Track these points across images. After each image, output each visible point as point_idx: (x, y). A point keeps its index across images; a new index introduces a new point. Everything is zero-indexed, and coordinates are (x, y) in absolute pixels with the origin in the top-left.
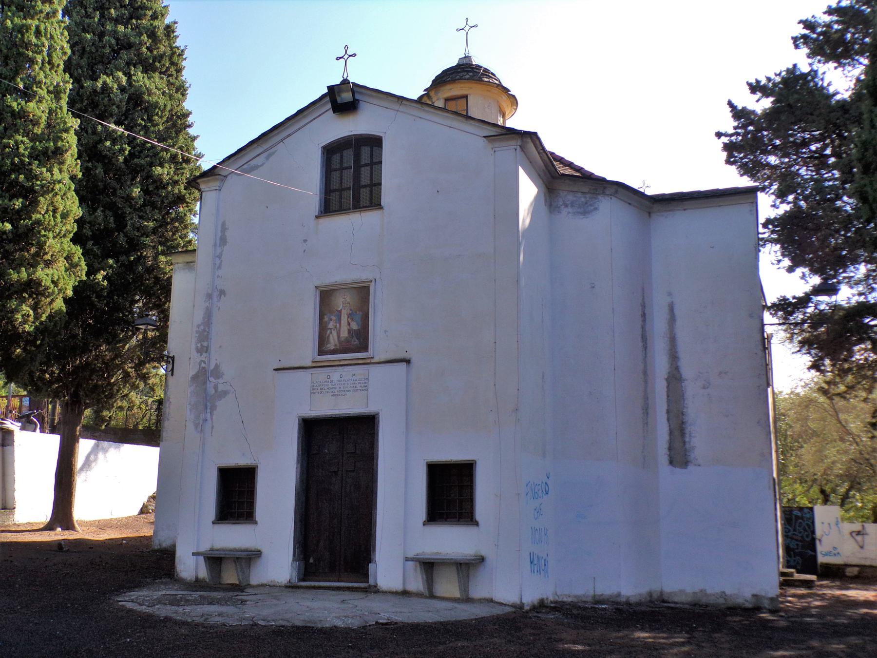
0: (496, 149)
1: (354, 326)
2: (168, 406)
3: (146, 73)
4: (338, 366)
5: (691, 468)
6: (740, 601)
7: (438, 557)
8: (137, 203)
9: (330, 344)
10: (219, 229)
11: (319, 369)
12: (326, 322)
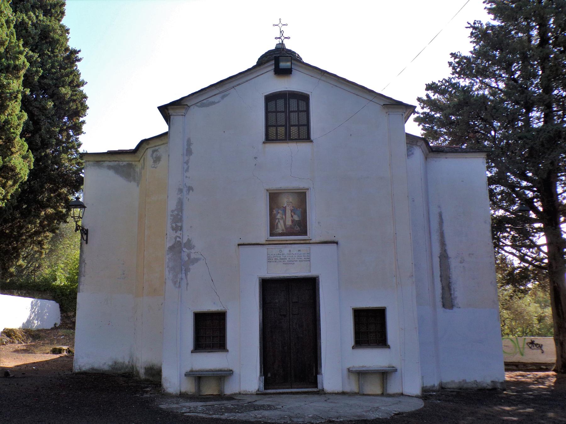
0: (390, 113)
1: (296, 218)
2: (83, 266)
3: (46, 16)
4: (287, 244)
5: (455, 309)
6: (485, 385)
7: (364, 369)
9: (278, 228)
10: (186, 144)
12: (275, 214)
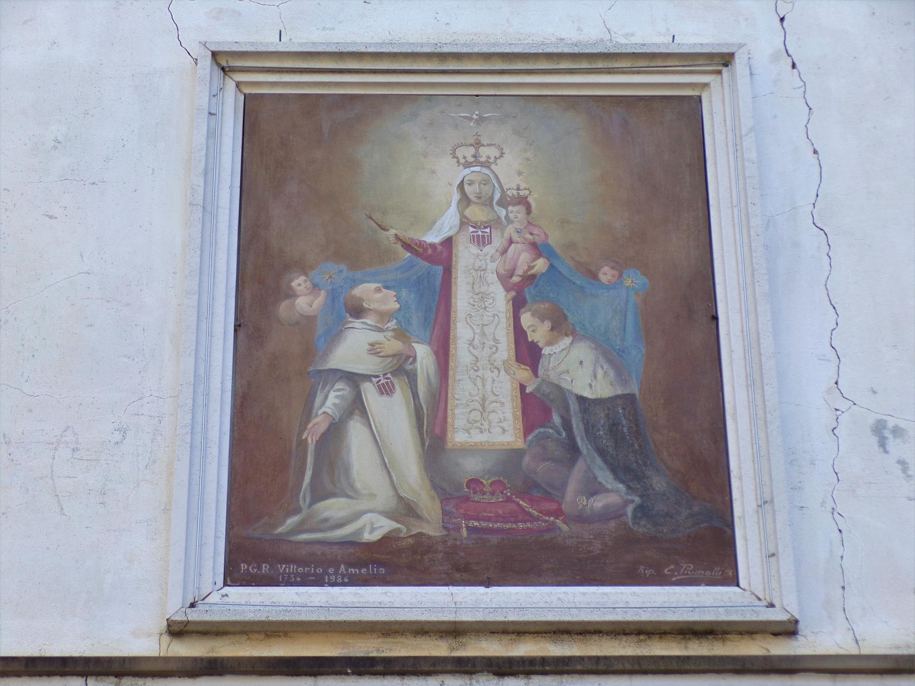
9: (351, 493)
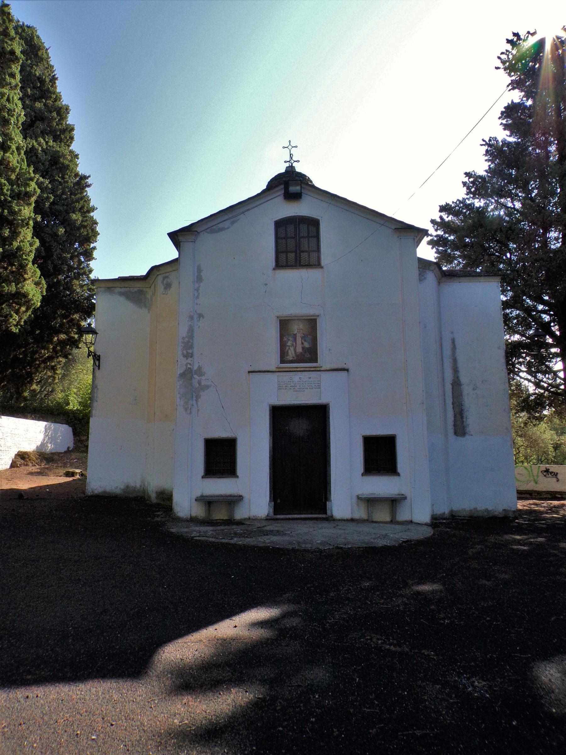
1: (307, 345)
5: (467, 437)
8: (61, 239)
11: (284, 373)
